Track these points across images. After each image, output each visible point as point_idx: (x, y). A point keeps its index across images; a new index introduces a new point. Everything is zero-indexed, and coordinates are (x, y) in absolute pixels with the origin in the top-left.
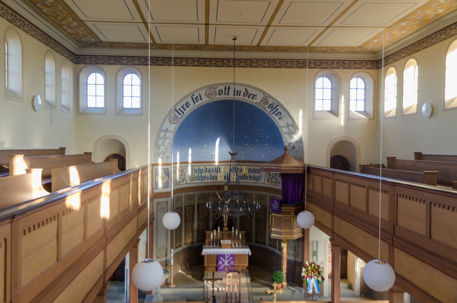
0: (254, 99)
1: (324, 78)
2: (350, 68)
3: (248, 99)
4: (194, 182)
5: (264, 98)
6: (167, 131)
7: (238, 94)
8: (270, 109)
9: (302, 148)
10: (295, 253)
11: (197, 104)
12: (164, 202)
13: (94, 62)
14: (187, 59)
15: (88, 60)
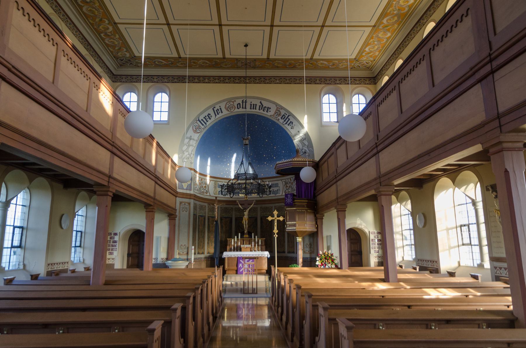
1: (330, 95)
3: (263, 112)
5: (277, 110)
6: (190, 139)
8: (283, 120)
10: (311, 250)
11: (218, 116)
12: (187, 203)
13: (129, 81)
15: (124, 79)
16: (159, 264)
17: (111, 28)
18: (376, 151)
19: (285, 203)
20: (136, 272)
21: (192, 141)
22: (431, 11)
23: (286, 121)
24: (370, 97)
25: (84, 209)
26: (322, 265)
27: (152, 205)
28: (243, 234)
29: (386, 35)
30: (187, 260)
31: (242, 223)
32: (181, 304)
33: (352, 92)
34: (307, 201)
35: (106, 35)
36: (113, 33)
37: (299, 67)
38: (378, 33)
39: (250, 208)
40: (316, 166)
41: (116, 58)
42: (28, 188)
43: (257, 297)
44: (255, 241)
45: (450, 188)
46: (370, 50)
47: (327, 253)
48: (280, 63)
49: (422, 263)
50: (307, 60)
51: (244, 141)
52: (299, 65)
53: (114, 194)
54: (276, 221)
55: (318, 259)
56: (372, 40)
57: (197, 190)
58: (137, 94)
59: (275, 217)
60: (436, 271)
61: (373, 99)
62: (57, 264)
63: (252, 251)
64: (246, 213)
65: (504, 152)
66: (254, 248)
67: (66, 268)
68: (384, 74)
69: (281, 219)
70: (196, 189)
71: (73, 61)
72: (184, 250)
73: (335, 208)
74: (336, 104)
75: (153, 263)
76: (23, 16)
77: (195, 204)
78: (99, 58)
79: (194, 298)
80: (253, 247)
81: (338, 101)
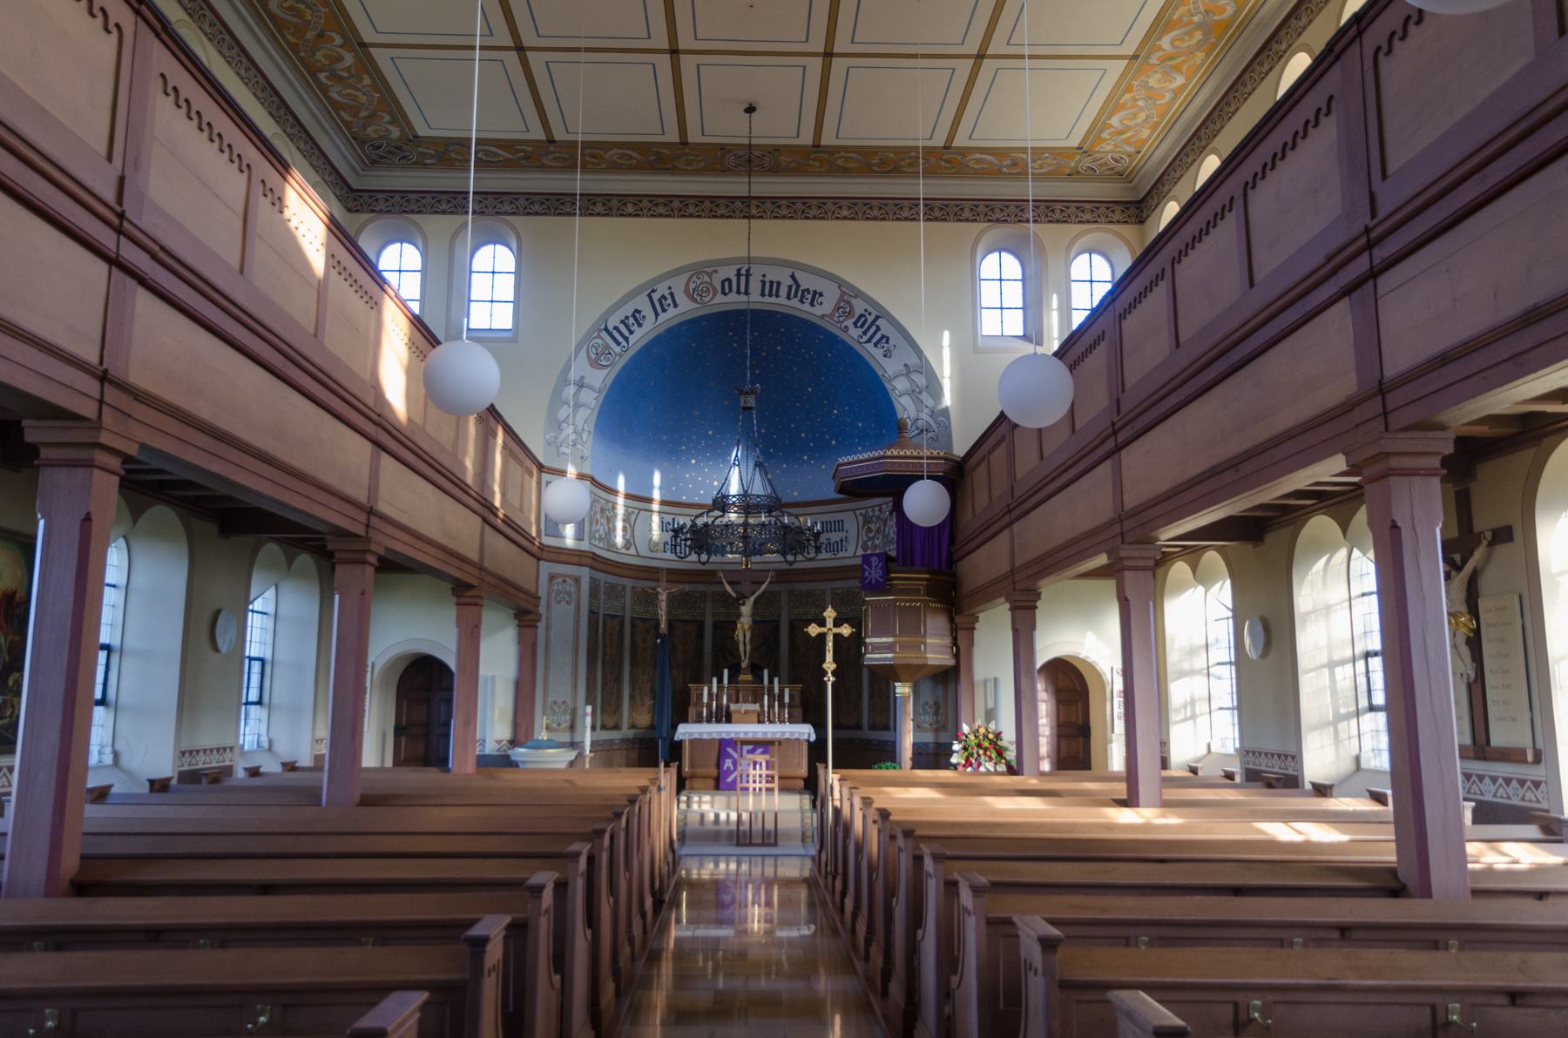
0: (815, 303)
2: (1066, 222)
3: (799, 305)
4: (660, 555)
5: (841, 299)
6: (581, 385)
7: (774, 293)
8: (860, 331)
9: (946, 427)
10: (937, 722)
11: (663, 317)
12: (569, 576)
14: (639, 198)
16: (489, 756)
17: (349, 59)
18: (1368, 267)
19: (863, 579)
20: (428, 777)
21: (584, 392)
22: (1300, 19)
23: (869, 334)
24: (1125, 262)
25: (270, 594)
26: (968, 763)
27: (474, 586)
28: (735, 671)
29: (1171, 82)
30: (573, 745)
31: (733, 638)
32: (554, 875)
33: (1069, 248)
34: (927, 576)
35: (334, 76)
36: (353, 71)
37: (911, 170)
38: (1148, 76)
39: (756, 594)
40: (954, 476)
41: (360, 140)
42: (124, 537)
43: (776, 856)
44: (771, 690)
45: (1341, 547)
46: (1124, 122)
47: (982, 730)
48: (852, 158)
49: (1257, 763)
50: (929, 151)
51: (742, 400)
52: (910, 165)
53: (380, 559)
54: (830, 638)
55: (956, 747)
56: (1128, 96)
57: (601, 539)
58: (421, 248)
59: (829, 627)
60: (1290, 782)
61: (1355, 28)
62: (205, 751)
63: (763, 722)
64: (746, 609)
65: (1391, 478)
66: (769, 712)
67: (227, 763)
68: (1167, 193)
69: (846, 630)
70: (597, 535)
71: (225, 144)
72: (563, 718)
73: (1007, 600)
74: (1020, 283)
75: (478, 753)
76: (175, 107)
77: (593, 580)
78: (310, 142)
79: (591, 860)
80: (766, 709)
81: (1027, 274)
